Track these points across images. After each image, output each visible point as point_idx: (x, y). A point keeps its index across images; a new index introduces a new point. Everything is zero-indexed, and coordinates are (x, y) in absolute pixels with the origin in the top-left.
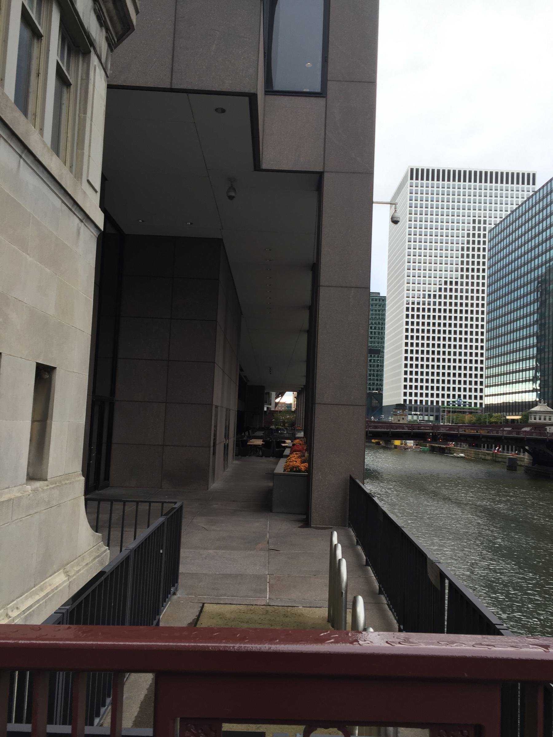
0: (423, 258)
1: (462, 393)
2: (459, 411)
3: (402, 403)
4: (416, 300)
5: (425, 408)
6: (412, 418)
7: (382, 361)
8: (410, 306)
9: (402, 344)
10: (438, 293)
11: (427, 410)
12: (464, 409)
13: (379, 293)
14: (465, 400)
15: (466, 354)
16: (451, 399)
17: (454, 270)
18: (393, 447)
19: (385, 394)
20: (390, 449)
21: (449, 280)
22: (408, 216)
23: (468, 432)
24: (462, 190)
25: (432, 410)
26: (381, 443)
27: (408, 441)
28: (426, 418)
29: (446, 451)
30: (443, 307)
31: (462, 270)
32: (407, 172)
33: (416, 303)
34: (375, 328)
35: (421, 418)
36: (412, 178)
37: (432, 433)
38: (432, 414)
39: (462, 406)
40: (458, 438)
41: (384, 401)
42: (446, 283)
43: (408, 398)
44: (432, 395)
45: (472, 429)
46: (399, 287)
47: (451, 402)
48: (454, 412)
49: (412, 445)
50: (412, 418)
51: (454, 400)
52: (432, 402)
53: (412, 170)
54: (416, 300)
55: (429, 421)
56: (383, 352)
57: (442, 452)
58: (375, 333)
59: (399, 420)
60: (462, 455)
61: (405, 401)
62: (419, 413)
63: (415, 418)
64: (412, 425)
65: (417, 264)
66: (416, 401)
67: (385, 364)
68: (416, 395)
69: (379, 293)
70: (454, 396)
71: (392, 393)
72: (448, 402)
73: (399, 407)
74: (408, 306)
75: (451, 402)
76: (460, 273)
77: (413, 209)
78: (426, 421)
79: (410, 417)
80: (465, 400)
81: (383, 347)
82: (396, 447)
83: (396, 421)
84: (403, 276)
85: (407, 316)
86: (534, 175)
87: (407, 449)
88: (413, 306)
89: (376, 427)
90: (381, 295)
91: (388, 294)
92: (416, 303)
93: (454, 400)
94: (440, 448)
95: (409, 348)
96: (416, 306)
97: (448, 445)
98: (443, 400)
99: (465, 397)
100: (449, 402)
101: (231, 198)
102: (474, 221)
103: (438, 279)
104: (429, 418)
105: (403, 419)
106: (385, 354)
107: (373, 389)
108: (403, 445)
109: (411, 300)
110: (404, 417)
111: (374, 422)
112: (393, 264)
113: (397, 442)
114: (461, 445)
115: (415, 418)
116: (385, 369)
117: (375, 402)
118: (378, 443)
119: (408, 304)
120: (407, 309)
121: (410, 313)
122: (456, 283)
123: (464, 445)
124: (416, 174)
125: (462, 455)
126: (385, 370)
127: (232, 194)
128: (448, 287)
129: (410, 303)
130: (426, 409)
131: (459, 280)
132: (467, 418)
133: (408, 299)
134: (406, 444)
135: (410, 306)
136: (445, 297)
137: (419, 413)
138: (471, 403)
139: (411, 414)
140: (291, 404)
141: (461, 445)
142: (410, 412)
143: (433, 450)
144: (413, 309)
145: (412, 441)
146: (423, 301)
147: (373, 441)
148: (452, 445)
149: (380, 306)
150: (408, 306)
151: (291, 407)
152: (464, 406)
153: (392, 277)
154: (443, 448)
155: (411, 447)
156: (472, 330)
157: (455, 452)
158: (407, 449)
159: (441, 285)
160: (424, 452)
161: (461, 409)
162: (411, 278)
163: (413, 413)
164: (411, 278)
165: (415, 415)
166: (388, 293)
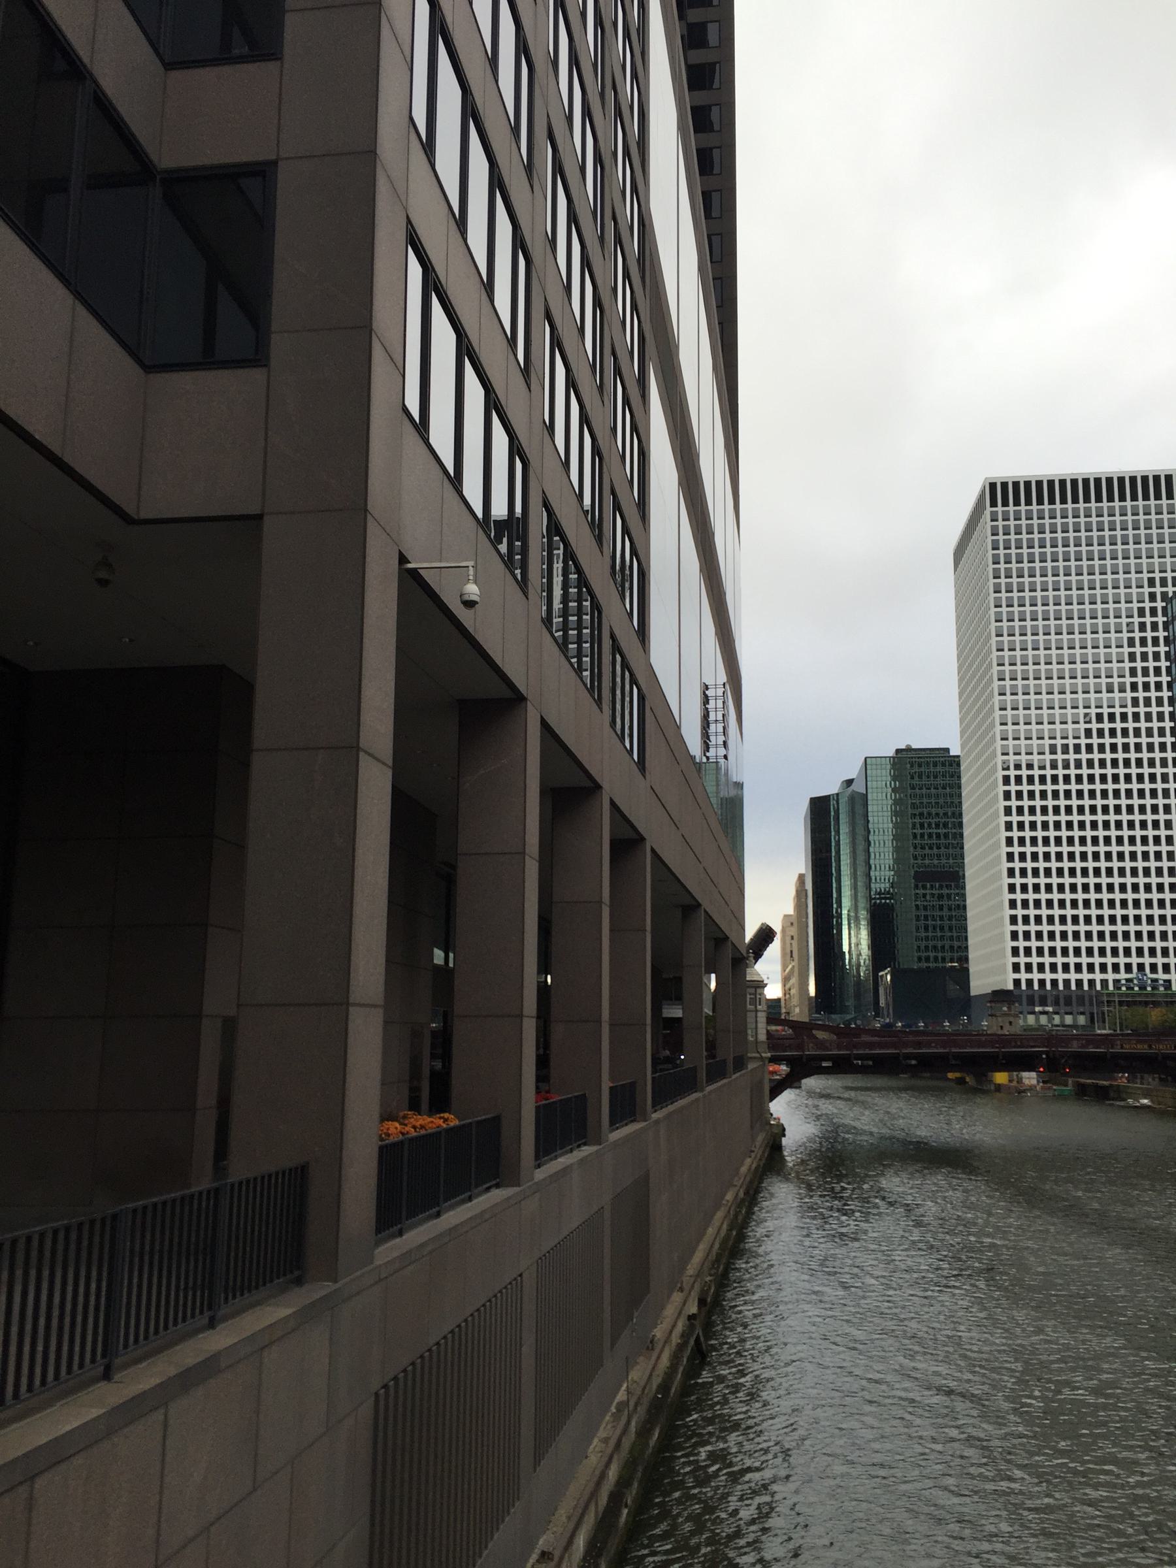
0: (1031, 667)
3: (1011, 987)
4: (1024, 759)
5: (1040, 996)
6: (1037, 1020)
8: (1012, 773)
9: (999, 856)
10: (1083, 741)
11: (1068, 1002)
12: (1153, 995)
13: (947, 750)
14: (1154, 976)
15: (1147, 872)
16: (1123, 975)
17: (1104, 689)
18: (993, 1088)
19: (974, 968)
20: (985, 1092)
21: (1105, 711)
22: (992, 581)
23: (1127, 1049)
26: (968, 1079)
27: (1025, 1074)
28: (1069, 1020)
29: (1112, 1094)
30: (1073, 772)
32: (983, 491)
33: (1024, 766)
34: (937, 826)
35: (1057, 1019)
36: (994, 503)
37: (1047, 1053)
38: (1068, 1009)
39: (1149, 989)
41: (973, 984)
42: (1100, 718)
43: (1023, 976)
44: (1078, 968)
47: (1123, 982)
48: (1128, 1004)
49: (1034, 1082)
50: (1037, 1020)
51: (1129, 976)
53: (993, 486)
54: (1024, 759)
55: (1074, 1026)
57: (1102, 1095)
60: (1145, 1101)
61: (1017, 982)
62: (1050, 1009)
63: (1043, 1020)
65: (1020, 682)
66: (1042, 982)
67: (969, 901)
68: (1066, 968)
69: (947, 750)
70: (1128, 968)
71: (991, 965)
72: (1116, 982)
73: (1000, 996)
74: (1006, 773)
76: (1129, 695)
77: (1002, 566)
78: (1069, 1026)
79: (1031, 1019)
80: (1154, 976)
81: (962, 866)
82: (999, 1088)
83: (995, 1030)
86: (1169, 478)
87: (1024, 1091)
88: (1018, 773)
89: (919, 1044)
90: (952, 753)
91: (962, 751)
92: (1024, 766)
94: (1096, 1086)
98: (1054, 976)
99: (1154, 968)
101: (103, 583)
104: (1075, 1020)
105: (1011, 1023)
107: (952, 961)
108: (1014, 1084)
109: (1012, 758)
110: (1011, 1019)
113: (1001, 1078)
114: (1142, 1078)
115: (1043, 1020)
117: (953, 988)
118: (961, 1081)
119: (1008, 769)
120: (1006, 780)
122: (1124, 717)
123: (1149, 1078)
124: (999, 493)
125: (1145, 1101)
126: (969, 915)
127: (103, 574)
128: (1106, 726)
129: (1012, 767)
130: (1065, 999)
131: (1130, 710)
132: (1155, 1015)
133: (1005, 757)
134: (1020, 1081)
135: (1012, 773)
136: (1102, 748)
137: (1050, 1009)
139: (1033, 1013)
140: (779, 1000)
141: (1142, 1078)
142: (1030, 1008)
143: (1082, 1092)
144: (1018, 780)
145: (1034, 1074)
147: (950, 1075)
148: (1122, 1079)
149: (952, 776)
151: (780, 1007)
152: (1154, 988)
155: (1031, 1088)
157: (1130, 1095)
158: (1024, 1091)
159: (1090, 722)
160: (1061, 1097)
162: (1009, 712)
163: (1037, 1009)
164: (1009, 712)
166: (963, 747)
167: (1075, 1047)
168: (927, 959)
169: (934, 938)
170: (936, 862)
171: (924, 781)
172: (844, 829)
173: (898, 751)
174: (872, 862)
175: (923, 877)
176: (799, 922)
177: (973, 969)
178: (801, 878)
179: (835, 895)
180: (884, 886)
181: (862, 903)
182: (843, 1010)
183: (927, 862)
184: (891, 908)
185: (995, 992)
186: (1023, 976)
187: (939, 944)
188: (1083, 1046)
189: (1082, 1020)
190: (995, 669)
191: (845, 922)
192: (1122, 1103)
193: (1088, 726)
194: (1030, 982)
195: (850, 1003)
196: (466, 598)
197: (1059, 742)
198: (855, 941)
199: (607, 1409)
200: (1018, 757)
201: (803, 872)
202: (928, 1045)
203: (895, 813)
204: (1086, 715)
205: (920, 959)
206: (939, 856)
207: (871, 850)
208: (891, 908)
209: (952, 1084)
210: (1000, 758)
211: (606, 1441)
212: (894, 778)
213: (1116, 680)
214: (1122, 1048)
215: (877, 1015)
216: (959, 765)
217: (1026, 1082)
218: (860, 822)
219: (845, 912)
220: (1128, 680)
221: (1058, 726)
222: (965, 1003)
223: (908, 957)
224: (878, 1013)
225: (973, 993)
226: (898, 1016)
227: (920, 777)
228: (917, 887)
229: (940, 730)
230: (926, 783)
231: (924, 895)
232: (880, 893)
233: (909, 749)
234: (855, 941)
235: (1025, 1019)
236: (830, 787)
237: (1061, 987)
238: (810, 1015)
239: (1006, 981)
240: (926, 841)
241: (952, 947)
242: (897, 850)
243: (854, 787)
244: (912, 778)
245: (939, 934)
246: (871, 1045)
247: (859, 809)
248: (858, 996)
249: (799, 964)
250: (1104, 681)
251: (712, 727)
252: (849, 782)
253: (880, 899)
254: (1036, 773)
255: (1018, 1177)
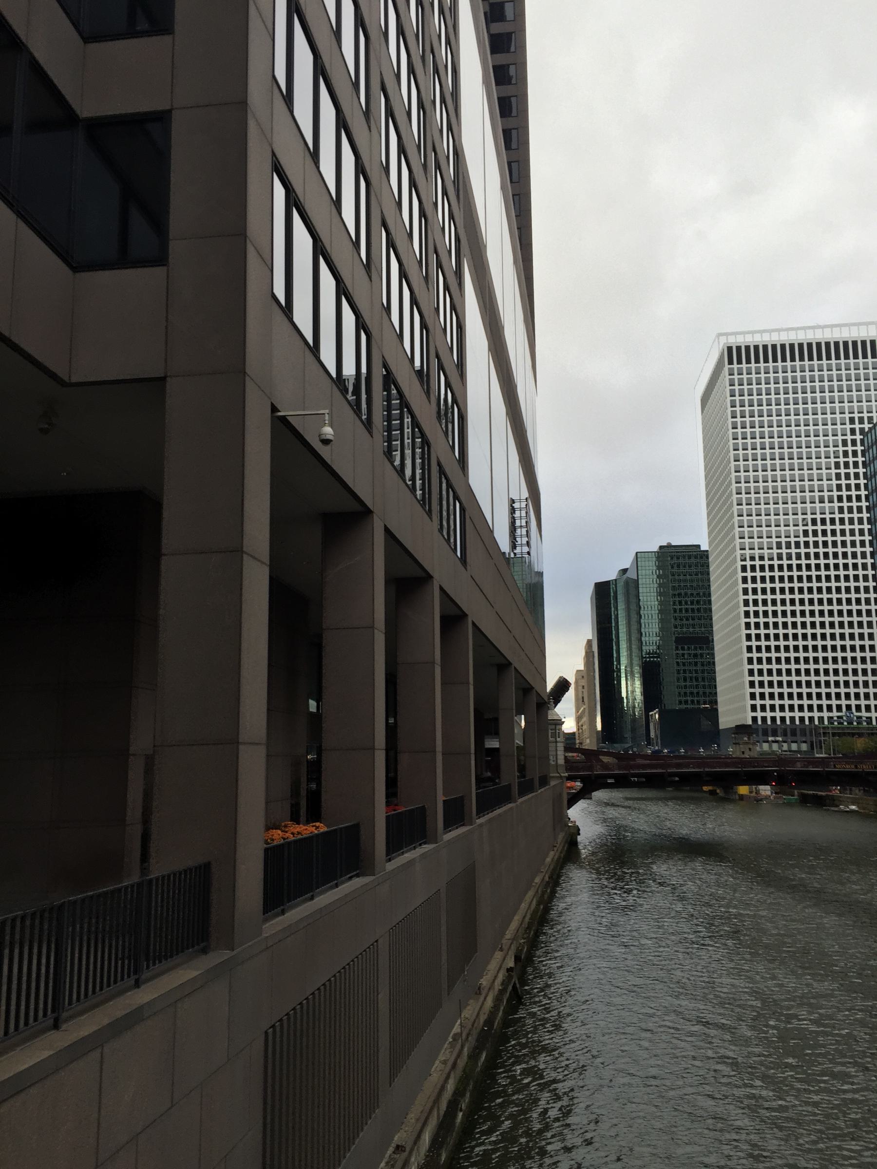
1: (853, 702)
2: (845, 731)
3: (750, 723)
5: (791, 729)
6: (770, 747)
7: (713, 655)
8: (748, 563)
10: (802, 539)
11: (794, 733)
12: (858, 728)
13: (699, 546)
14: (859, 714)
16: (835, 714)
18: (737, 797)
19: (721, 709)
21: (818, 517)
23: (839, 768)
24: (798, 374)
25: (803, 732)
26: (718, 791)
27: (761, 787)
28: (794, 747)
29: (828, 801)
31: (840, 499)
35: (785, 746)
36: (731, 362)
38: (794, 739)
39: (855, 723)
40: (848, 780)
41: (721, 720)
43: (759, 714)
45: (847, 763)
46: (727, 534)
47: (835, 718)
48: (839, 735)
49: (769, 793)
50: (770, 747)
51: (839, 714)
52: (802, 719)
53: (730, 349)
55: (799, 751)
56: (713, 641)
57: (820, 803)
58: (693, 610)
59: (743, 753)
60: (853, 807)
61: (754, 719)
63: (775, 747)
64: (764, 759)
67: (716, 659)
69: (699, 546)
70: (839, 708)
71: (734, 707)
72: (830, 718)
73: (741, 729)
74: (744, 563)
75: (835, 718)
76: (836, 505)
79: (766, 746)
80: (859, 714)
82: (742, 797)
83: (738, 754)
84: (732, 516)
85: (745, 580)
87: (761, 800)
90: (702, 549)
93: (839, 714)
95: (753, 632)
96: (757, 563)
97: (830, 791)
100: (832, 718)
102: (852, 421)
103: (800, 517)
104: (799, 747)
105: (750, 749)
106: (715, 643)
107: (705, 703)
108: (754, 794)
109: (748, 552)
110: (751, 746)
111: (702, 758)
112: (713, 498)
113: (743, 790)
114: (851, 790)
115: (775, 747)
116: (717, 669)
117: (705, 724)
118: (712, 793)
119: (745, 560)
121: (749, 574)
122: (833, 521)
123: (856, 790)
124: (735, 355)
125: (853, 807)
129: (748, 559)
130: (792, 731)
131: (837, 516)
132: (860, 744)
134: (757, 792)
135: (748, 563)
137: (780, 739)
138: (870, 718)
139: (767, 742)
140: (574, 734)
141: (851, 790)
143: (805, 801)
145: (768, 787)
146: (778, 554)
147: (705, 788)
148: (836, 791)
150: (744, 563)
151: (575, 739)
153: (714, 518)
154: (821, 796)
156: (755, 597)
158: (761, 800)
160: (789, 804)
161: (854, 728)
163: (770, 739)
164: (745, 518)
165: (773, 742)
166: (710, 544)
167: (799, 767)
168: (686, 702)
169: (691, 686)
170: (691, 630)
171: (682, 570)
172: (621, 606)
173: (661, 547)
174: (643, 630)
175: (681, 641)
176: (588, 675)
177: (721, 709)
178: (589, 642)
179: (615, 655)
180: (652, 648)
181: (636, 661)
182: (622, 740)
183: (684, 630)
184: (658, 665)
185: (738, 727)
186: (759, 714)
187: (695, 691)
188: (805, 766)
189: (804, 747)
190: (734, 485)
191: (623, 675)
192: (836, 809)
193: (805, 528)
194: (764, 719)
195: (628, 735)
196: (323, 437)
197: (783, 540)
198: (631, 689)
199: (446, 1039)
200: (752, 551)
201: (591, 638)
202: (687, 766)
203: (660, 594)
204: (804, 519)
205: (680, 702)
206: (693, 626)
207: (642, 621)
208: (658, 665)
209: (708, 795)
210: (739, 552)
211: (445, 1062)
212: (659, 568)
213: (826, 494)
214: (835, 767)
215: (649, 744)
216: (707, 557)
217: (763, 793)
218: (633, 600)
219: (623, 668)
220: (835, 494)
221: (782, 528)
222: (714, 734)
223: (671, 701)
224: (649, 742)
225: (721, 727)
226: (664, 745)
227: (678, 566)
228: (677, 649)
229: (695, 533)
230: (683, 570)
231: (683, 655)
232: (649, 654)
233: (669, 546)
234: (631, 689)
235: (761, 747)
236: (610, 575)
237: (788, 722)
238: (598, 744)
239: (746, 719)
240: (684, 614)
241: (704, 693)
242: (661, 621)
243: (628, 574)
244: (672, 567)
245: (695, 683)
246: (644, 767)
247: (632, 592)
248: (633, 730)
249: (589, 707)
250: (817, 494)
251: (518, 531)
252: (625, 571)
253: (650, 657)
254: (767, 563)
255: (756, 863)
